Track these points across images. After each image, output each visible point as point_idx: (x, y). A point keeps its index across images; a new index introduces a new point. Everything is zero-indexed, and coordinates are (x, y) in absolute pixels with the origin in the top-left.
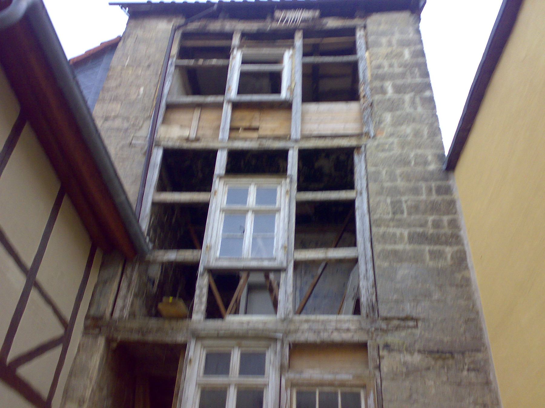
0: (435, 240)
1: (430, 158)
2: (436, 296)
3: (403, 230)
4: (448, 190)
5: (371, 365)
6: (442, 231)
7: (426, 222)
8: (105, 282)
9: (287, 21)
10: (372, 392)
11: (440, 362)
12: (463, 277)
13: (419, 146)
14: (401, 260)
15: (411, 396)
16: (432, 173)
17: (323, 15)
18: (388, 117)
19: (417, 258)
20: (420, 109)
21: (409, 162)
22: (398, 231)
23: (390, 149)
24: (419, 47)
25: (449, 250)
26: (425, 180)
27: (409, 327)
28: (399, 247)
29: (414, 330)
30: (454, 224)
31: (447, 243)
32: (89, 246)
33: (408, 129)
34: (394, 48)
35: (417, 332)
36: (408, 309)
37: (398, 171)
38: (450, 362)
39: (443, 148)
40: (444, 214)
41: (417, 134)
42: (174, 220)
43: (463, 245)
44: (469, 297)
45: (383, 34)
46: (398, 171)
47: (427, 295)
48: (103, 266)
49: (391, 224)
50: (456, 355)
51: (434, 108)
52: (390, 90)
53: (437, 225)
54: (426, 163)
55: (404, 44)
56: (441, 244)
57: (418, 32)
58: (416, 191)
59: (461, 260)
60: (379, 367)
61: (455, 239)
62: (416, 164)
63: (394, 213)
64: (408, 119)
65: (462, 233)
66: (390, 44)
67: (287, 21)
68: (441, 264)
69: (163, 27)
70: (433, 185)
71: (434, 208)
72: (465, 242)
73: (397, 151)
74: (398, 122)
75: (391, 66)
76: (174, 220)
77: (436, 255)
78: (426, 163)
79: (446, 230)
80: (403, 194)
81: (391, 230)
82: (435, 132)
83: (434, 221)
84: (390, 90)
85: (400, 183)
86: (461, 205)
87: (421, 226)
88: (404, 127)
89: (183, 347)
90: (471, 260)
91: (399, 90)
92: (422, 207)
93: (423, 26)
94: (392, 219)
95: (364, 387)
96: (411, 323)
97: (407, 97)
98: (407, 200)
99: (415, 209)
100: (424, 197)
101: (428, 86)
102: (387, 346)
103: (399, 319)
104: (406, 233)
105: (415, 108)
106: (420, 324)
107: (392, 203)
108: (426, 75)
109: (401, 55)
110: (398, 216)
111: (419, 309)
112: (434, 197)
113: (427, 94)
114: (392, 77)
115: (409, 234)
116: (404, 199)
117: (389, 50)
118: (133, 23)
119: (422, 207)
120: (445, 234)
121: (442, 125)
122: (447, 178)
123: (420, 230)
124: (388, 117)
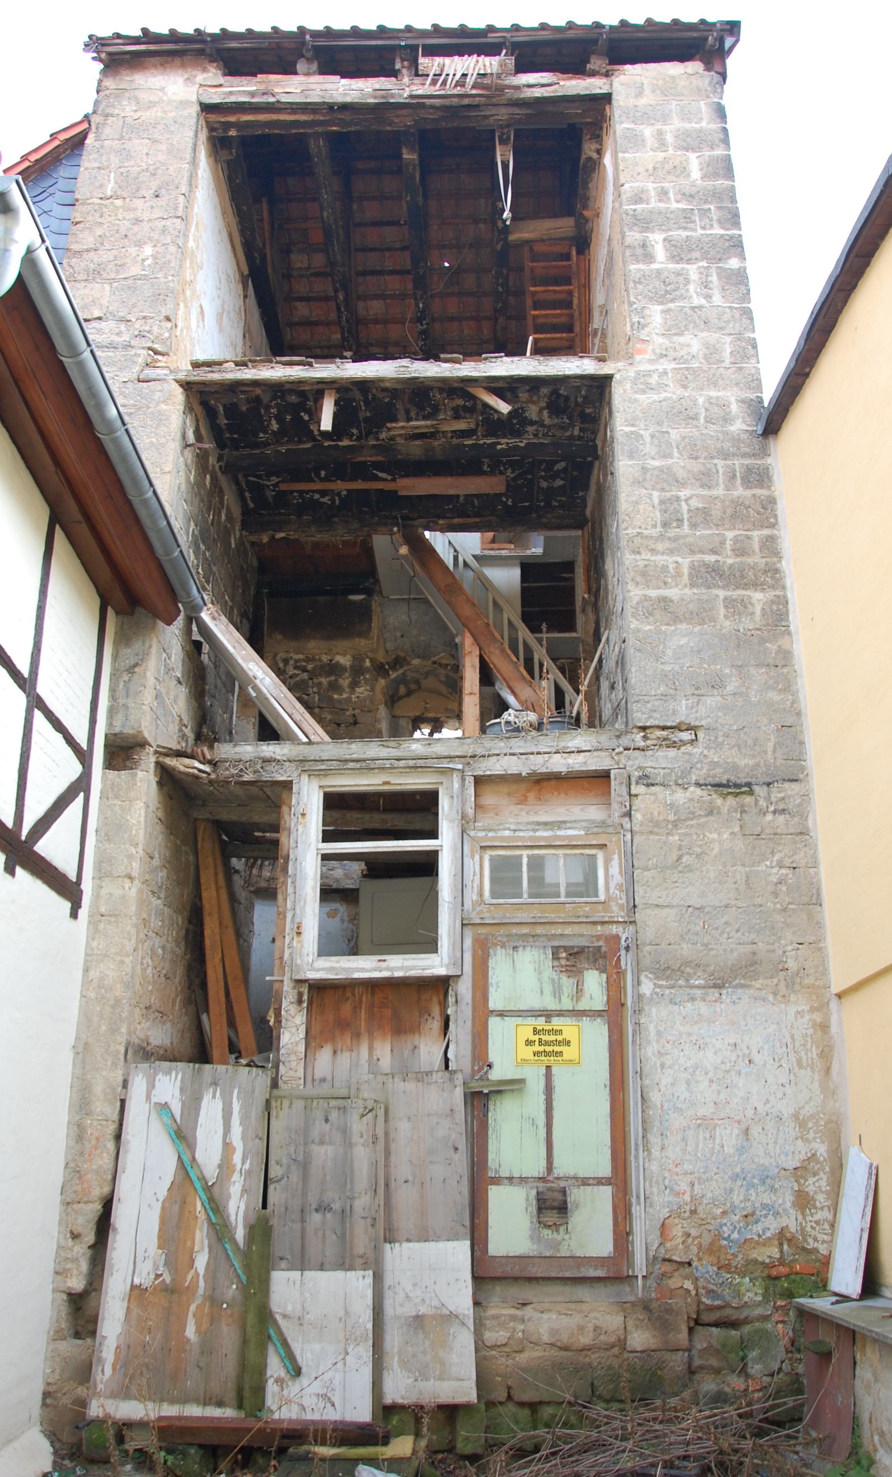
0: (736, 578)
1: (734, 408)
2: (732, 686)
3: (680, 560)
4: (760, 477)
5: (617, 810)
6: (749, 560)
7: (723, 543)
8: (131, 670)
9: (444, 83)
10: (616, 857)
11: (731, 801)
12: (780, 650)
13: (714, 383)
14: (676, 620)
15: (680, 858)
16: (736, 440)
17: (521, 68)
18: (656, 314)
19: (701, 615)
20: (717, 299)
21: (695, 418)
22: (669, 561)
23: (661, 387)
24: (719, 152)
25: (758, 597)
26: (726, 456)
27: (684, 743)
28: (673, 593)
29: (689, 748)
30: (771, 546)
31: (756, 585)
32: (97, 601)
33: (693, 343)
34: (671, 151)
35: (697, 750)
36: (682, 710)
37: (674, 435)
38: (748, 799)
39: (759, 388)
40: (755, 527)
41: (712, 353)
42: (223, 518)
43: (784, 588)
44: (788, 686)
45: (645, 117)
46: (674, 435)
47: (717, 684)
48: (123, 639)
49: (660, 547)
50: (756, 789)
51: (746, 296)
52: (660, 253)
53: (741, 550)
54: (727, 419)
55: (690, 142)
56: (746, 587)
57: (721, 112)
58: (705, 479)
59: (778, 617)
60: (629, 814)
61: (771, 576)
62: (709, 420)
63: (665, 525)
64: (695, 320)
65: (784, 565)
66: (662, 145)
67: (444, 83)
68: (746, 624)
69: (179, 92)
70: (738, 463)
71: (737, 514)
72: (788, 582)
73: (673, 392)
74: (673, 330)
75: (663, 194)
76: (223, 518)
77: (736, 607)
78: (727, 419)
79: (757, 559)
80: (681, 484)
81: (660, 559)
82: (747, 349)
83: (736, 540)
84: (660, 253)
85: (678, 462)
86: (783, 508)
87: (714, 552)
88: (686, 338)
89: (287, 785)
90: (796, 618)
91: (678, 252)
92: (716, 513)
93: (731, 96)
94: (661, 537)
95: (602, 846)
96: (686, 736)
97: (693, 271)
98: (691, 496)
99: (702, 516)
100: (720, 491)
101: (737, 246)
102: (647, 780)
103: (664, 728)
104: (685, 562)
105: (708, 297)
106: (701, 735)
107: (662, 502)
108: (733, 218)
109: (682, 170)
110: (672, 533)
111: (702, 710)
112: (739, 491)
113: (734, 263)
114: (664, 221)
115: (692, 567)
116: (684, 493)
117: (660, 155)
118: (109, 83)
119: (716, 513)
120: (753, 567)
121: (760, 335)
122: (764, 452)
123: (712, 558)
124: (656, 314)
